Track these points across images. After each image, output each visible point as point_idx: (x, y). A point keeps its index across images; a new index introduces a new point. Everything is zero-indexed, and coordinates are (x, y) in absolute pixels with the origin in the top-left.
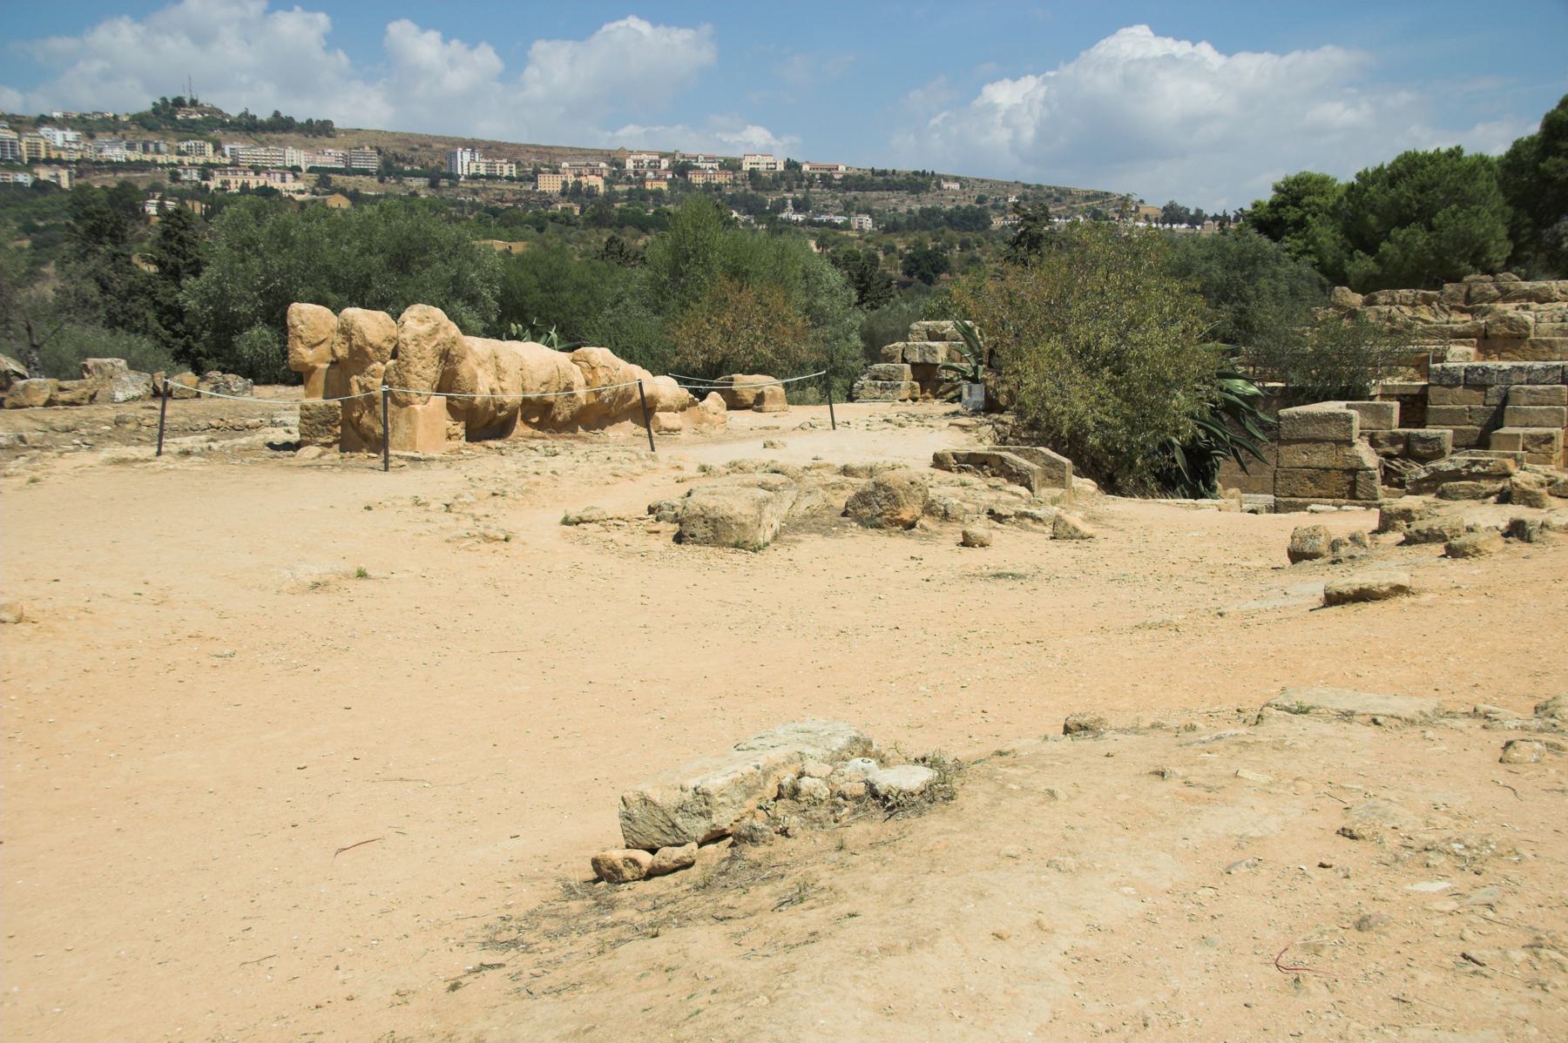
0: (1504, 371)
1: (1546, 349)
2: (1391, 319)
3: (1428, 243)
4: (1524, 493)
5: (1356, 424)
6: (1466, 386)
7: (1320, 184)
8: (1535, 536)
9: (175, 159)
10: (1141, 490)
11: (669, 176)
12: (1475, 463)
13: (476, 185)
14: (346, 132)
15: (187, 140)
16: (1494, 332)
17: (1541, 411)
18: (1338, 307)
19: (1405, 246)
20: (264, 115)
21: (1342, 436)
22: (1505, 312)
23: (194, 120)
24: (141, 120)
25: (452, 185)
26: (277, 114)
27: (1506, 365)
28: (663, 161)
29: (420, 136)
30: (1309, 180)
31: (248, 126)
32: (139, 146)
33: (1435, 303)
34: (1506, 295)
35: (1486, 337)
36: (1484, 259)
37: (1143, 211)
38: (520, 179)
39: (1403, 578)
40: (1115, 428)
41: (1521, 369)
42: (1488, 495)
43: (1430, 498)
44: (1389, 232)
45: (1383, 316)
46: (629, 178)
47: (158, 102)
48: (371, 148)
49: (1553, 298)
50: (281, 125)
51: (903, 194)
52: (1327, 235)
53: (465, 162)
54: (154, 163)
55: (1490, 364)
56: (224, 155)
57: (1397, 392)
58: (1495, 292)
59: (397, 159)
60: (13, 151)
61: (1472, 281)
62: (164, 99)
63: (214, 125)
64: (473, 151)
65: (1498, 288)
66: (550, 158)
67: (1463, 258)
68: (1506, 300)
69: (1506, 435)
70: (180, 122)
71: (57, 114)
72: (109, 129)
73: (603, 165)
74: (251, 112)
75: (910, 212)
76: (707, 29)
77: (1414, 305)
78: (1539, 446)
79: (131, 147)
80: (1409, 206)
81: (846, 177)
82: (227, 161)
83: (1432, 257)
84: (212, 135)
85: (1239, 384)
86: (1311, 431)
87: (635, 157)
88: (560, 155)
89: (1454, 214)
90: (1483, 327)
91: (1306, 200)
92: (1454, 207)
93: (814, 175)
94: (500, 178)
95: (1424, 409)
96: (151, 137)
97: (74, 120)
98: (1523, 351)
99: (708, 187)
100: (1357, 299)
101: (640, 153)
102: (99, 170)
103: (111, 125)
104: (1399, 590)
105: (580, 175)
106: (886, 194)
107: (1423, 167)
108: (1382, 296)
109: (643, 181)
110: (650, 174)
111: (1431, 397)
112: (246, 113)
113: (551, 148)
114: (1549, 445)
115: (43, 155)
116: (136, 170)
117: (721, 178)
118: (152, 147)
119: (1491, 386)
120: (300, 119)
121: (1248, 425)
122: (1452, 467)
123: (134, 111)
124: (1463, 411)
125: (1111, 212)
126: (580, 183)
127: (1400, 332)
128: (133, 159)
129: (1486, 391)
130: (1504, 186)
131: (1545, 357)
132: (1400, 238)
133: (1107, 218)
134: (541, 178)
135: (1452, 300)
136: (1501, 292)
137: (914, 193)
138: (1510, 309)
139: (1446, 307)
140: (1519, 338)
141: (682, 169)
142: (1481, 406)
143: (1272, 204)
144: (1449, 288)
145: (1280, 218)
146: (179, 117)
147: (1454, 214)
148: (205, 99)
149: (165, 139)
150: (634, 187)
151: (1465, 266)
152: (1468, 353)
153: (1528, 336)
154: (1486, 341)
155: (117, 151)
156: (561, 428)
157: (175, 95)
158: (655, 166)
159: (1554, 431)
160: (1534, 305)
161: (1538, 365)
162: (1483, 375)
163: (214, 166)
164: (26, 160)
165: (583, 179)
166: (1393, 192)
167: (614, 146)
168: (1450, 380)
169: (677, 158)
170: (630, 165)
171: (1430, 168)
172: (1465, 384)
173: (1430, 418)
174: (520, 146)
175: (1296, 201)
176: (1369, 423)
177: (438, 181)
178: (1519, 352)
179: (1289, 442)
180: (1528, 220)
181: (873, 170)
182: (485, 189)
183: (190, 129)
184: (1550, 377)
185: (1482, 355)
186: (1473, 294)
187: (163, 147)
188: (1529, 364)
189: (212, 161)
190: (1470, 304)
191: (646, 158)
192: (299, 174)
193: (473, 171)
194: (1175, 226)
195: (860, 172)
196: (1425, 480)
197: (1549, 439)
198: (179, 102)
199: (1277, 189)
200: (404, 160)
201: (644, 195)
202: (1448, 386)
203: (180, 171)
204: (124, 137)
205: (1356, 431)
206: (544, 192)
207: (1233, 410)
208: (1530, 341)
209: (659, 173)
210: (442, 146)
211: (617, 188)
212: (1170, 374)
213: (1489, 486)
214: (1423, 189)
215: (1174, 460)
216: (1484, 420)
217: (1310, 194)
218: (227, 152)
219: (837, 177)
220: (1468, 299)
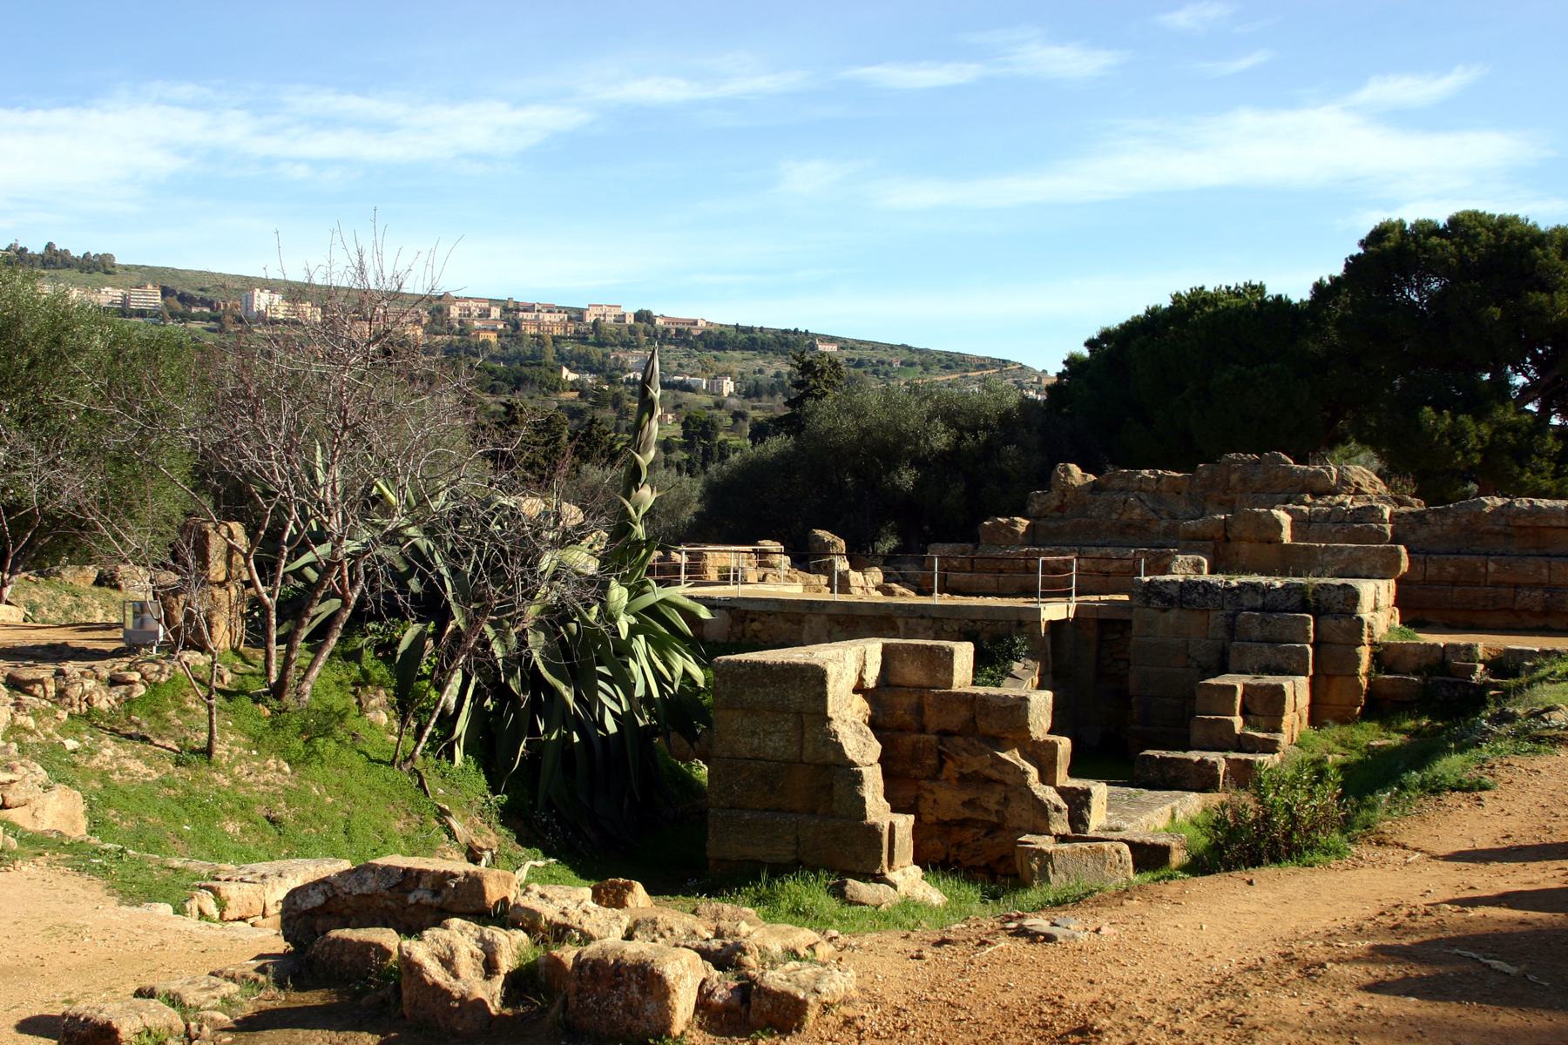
14: (126, 268)
20: (36, 247)
26: (50, 246)
28: (493, 309)
75: (778, 375)
87: (461, 304)
93: (668, 330)
120: (77, 252)
158: (485, 314)
170: (455, 312)
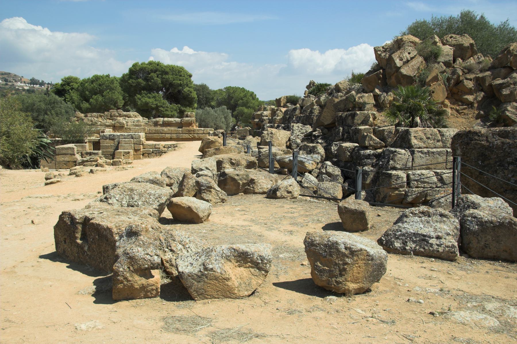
2: (92, 121)
3: (102, 100)
4: (100, 164)
5: (76, 150)
6: (109, 139)
7: (75, 80)
8: (94, 172)
10: (17, 168)
12: (91, 158)
18: (78, 118)
19: (96, 100)
21: (72, 153)
22: (120, 120)
27: (119, 134)
30: (72, 78)
34: (120, 116)
35: (114, 126)
37: (23, 80)
39: (59, 179)
40: (8, 152)
41: (122, 135)
42: (93, 165)
43: (82, 166)
44: (92, 96)
52: (75, 96)
55: (115, 134)
57: (92, 141)
58: (117, 114)
67: (111, 104)
68: (120, 117)
77: (97, 117)
80: (97, 89)
85: (45, 140)
86: (64, 152)
89: (108, 93)
91: (71, 84)
92: (108, 91)
95: (99, 146)
100: (82, 115)
104: (58, 181)
107: (100, 79)
108: (89, 115)
111: (101, 142)
121: (48, 150)
122: (86, 159)
124: (109, 146)
125: (11, 79)
127: (94, 124)
130: (121, 86)
132: (95, 98)
133: (10, 82)
138: (121, 119)
143: (61, 85)
144: (106, 113)
145: (64, 89)
147: (108, 93)
151: (112, 107)
154: (114, 128)
159: (130, 151)
160: (127, 118)
161: (126, 134)
166: (92, 85)
168: (105, 138)
171: (102, 79)
173: (101, 148)
175: (68, 84)
176: (80, 149)
179: (59, 155)
180: (127, 95)
186: (112, 115)
188: (124, 133)
190: (112, 117)
194: (35, 86)
196: (81, 162)
197: (129, 153)
199: (62, 80)
205: (76, 152)
207: (42, 146)
212: (24, 138)
213: (94, 163)
214: (100, 85)
215: (27, 160)
216: (114, 148)
217: (72, 82)
220: (111, 116)
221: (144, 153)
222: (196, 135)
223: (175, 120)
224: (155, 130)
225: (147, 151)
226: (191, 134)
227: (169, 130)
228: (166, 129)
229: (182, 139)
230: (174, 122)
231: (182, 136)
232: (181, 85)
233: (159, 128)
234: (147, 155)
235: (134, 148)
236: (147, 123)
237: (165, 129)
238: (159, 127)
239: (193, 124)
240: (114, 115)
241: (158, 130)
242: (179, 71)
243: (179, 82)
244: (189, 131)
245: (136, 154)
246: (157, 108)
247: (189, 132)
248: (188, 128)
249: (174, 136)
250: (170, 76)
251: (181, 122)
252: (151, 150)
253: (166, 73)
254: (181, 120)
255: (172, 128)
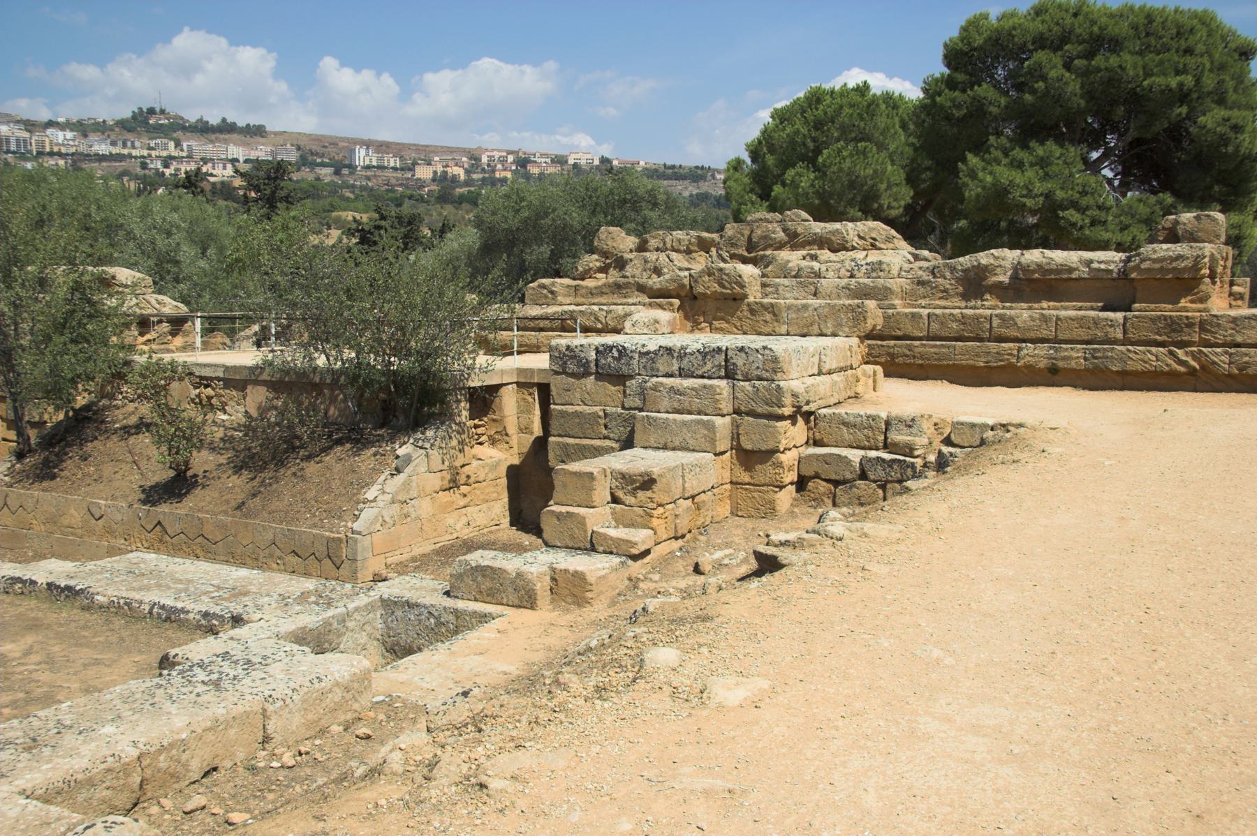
0: (648, 353)
1: (768, 317)
6: (600, 376)
9: (145, 153)
11: (514, 168)
13: (369, 173)
14: (276, 134)
15: (156, 138)
16: (700, 289)
17: (684, 423)
18: (605, 254)
20: (214, 120)
23: (162, 125)
24: (123, 125)
25: (351, 173)
26: (224, 120)
29: (331, 137)
31: (203, 129)
32: (120, 143)
33: (714, 250)
34: (794, 241)
36: (876, 205)
38: (402, 169)
41: (669, 350)
45: (648, 266)
46: (483, 169)
47: (136, 111)
48: (292, 145)
49: (848, 245)
50: (227, 128)
51: (686, 182)
53: (362, 157)
54: (130, 156)
56: (182, 150)
58: (781, 235)
59: (312, 154)
60: (25, 146)
61: (756, 221)
62: (141, 109)
63: (177, 128)
64: (368, 148)
65: (784, 230)
66: (425, 154)
68: (794, 247)
69: (575, 474)
70: (151, 125)
71: (61, 120)
72: (99, 131)
73: (464, 159)
74: (205, 119)
75: (691, 195)
76: (551, 65)
77: (688, 252)
78: (633, 493)
79: (114, 144)
80: (804, 144)
81: (645, 169)
82: (184, 154)
83: (817, 202)
84: (175, 135)
88: (432, 152)
90: (686, 282)
94: (387, 168)
96: (130, 136)
97: (74, 124)
98: (740, 319)
99: (541, 176)
101: (493, 150)
102: (89, 160)
103: (101, 128)
105: (447, 166)
106: (674, 182)
109: (493, 171)
110: (499, 166)
112: (201, 119)
113: (427, 146)
114: (649, 493)
115: (48, 150)
116: (116, 161)
117: (552, 170)
118: (129, 144)
119: (631, 377)
120: (241, 123)
123: (118, 117)
126: (446, 172)
128: (114, 152)
129: (624, 385)
131: (769, 330)
134: (417, 168)
135: (733, 245)
136: (787, 235)
137: (694, 182)
139: (726, 255)
140: (735, 299)
141: (523, 162)
142: (619, 410)
146: (151, 122)
148: (172, 110)
149: (139, 138)
150: (487, 175)
152: (656, 322)
153: (746, 296)
155: (103, 147)
156: (494, 349)
157: (149, 106)
158: (503, 160)
160: (825, 254)
162: (618, 359)
163: (173, 158)
164: (35, 153)
165: (449, 170)
167: (474, 146)
169: (520, 154)
170: (485, 159)
172: (597, 373)
174: (403, 145)
177: (341, 170)
178: (735, 321)
181: (665, 165)
182: (375, 176)
183: (159, 131)
184: (709, 366)
185: (689, 324)
187: (137, 144)
189: (173, 154)
191: (497, 155)
192: (237, 164)
193: (367, 162)
195: (654, 167)
198: (151, 111)
200: (317, 154)
201: (493, 182)
202: (573, 375)
203: (148, 161)
204: (109, 136)
206: (420, 179)
208: (748, 305)
209: (506, 165)
210: (346, 144)
211: (475, 176)
218: (185, 148)
219: (639, 169)
220: (751, 246)
221: (808, 472)
222: (1219, 357)
223: (1088, 263)
224: (963, 320)
225: (825, 459)
226: (1181, 345)
227: (1045, 319)
228: (1026, 314)
229: (1123, 373)
230: (1084, 272)
231: (1123, 359)
232: (1183, 96)
233: (988, 308)
234: (823, 487)
235: (736, 437)
236: (926, 276)
237: (1023, 313)
238: (990, 300)
239: (1206, 285)
240: (765, 237)
241: (977, 317)
242: (1179, 27)
243: (1173, 82)
244: (1173, 325)
245: (746, 477)
246: (1051, 208)
247: (1174, 336)
248: (1167, 310)
249: (1075, 356)
250: (1128, 59)
251: (1124, 274)
252: (855, 455)
253: (1115, 45)
254: (1129, 259)
255: (1068, 311)
